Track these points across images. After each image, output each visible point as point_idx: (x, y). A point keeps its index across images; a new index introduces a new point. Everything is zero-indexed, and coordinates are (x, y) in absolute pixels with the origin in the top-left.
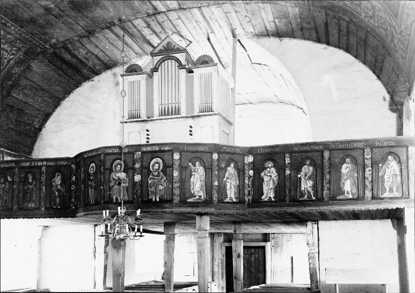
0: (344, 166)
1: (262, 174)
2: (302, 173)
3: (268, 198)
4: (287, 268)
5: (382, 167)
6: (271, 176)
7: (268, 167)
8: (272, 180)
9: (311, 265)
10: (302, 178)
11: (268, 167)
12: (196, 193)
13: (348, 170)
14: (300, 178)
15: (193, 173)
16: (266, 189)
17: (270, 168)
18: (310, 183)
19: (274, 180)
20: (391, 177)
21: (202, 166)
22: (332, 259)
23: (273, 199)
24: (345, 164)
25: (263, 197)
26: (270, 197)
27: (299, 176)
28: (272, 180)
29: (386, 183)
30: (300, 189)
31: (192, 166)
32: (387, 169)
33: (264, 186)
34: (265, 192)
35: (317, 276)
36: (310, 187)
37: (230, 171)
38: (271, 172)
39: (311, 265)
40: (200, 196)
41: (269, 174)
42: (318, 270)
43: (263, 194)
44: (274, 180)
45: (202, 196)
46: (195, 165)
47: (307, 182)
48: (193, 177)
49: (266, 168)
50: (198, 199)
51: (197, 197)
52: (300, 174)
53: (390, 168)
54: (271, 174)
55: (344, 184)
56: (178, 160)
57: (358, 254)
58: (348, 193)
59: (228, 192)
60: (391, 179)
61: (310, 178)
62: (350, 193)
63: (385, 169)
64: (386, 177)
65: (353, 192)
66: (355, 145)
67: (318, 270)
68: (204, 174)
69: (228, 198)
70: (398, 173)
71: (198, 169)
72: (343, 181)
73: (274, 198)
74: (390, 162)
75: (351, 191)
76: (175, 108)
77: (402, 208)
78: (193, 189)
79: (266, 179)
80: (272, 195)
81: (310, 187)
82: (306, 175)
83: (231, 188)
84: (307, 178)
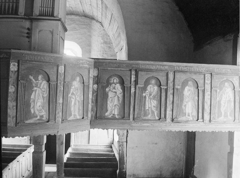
0: (187, 88)
1: (107, 90)
2: (147, 91)
3: (112, 115)
4: (86, 134)
5: (219, 92)
6: (116, 92)
7: (113, 83)
8: (116, 96)
9: (121, 152)
10: (147, 96)
11: (113, 83)
12: (37, 113)
13: (189, 92)
14: (145, 97)
15: (35, 88)
16: (111, 105)
17: (115, 84)
18: (154, 103)
19: (118, 97)
20: (226, 102)
21: (45, 80)
22: (137, 147)
23: (117, 117)
24: (187, 87)
25: (106, 114)
26: (114, 114)
27: (144, 95)
28: (116, 96)
29: (222, 108)
30: (145, 108)
31: (34, 80)
32: (223, 95)
33: (108, 102)
34: (109, 108)
35: (124, 160)
36: (154, 107)
37: (76, 86)
38: (116, 88)
39: (121, 152)
40: (42, 116)
41: (114, 90)
42: (125, 155)
43: (107, 111)
44: (118, 97)
45: (44, 116)
46: (37, 79)
47: (152, 101)
48: (34, 93)
49: (111, 84)
50: (39, 120)
51: (38, 118)
52: (145, 93)
53: (226, 94)
54: (116, 91)
55: (185, 106)
56: (15, 71)
57: (156, 144)
58: (189, 115)
59: (72, 109)
60: (226, 105)
61: (154, 97)
62: (190, 115)
63: (222, 95)
64: (222, 102)
65: (193, 114)
66: (197, 69)
67: (125, 155)
68: (48, 90)
69: (73, 116)
70: (233, 100)
71: (41, 84)
72: (185, 103)
73: (118, 115)
74: (226, 88)
75: (192, 113)
76: (9, 7)
77: (233, 131)
78: (34, 107)
79: (111, 95)
80: (116, 112)
81: (154, 107)
82: (150, 95)
83: (75, 104)
84: (151, 97)
